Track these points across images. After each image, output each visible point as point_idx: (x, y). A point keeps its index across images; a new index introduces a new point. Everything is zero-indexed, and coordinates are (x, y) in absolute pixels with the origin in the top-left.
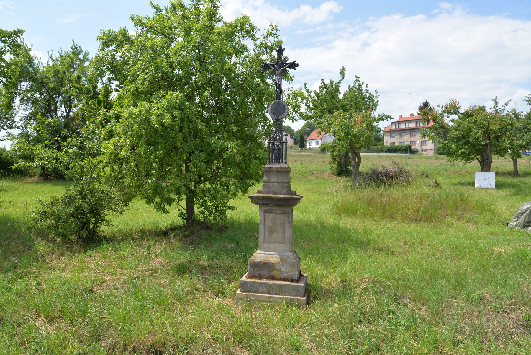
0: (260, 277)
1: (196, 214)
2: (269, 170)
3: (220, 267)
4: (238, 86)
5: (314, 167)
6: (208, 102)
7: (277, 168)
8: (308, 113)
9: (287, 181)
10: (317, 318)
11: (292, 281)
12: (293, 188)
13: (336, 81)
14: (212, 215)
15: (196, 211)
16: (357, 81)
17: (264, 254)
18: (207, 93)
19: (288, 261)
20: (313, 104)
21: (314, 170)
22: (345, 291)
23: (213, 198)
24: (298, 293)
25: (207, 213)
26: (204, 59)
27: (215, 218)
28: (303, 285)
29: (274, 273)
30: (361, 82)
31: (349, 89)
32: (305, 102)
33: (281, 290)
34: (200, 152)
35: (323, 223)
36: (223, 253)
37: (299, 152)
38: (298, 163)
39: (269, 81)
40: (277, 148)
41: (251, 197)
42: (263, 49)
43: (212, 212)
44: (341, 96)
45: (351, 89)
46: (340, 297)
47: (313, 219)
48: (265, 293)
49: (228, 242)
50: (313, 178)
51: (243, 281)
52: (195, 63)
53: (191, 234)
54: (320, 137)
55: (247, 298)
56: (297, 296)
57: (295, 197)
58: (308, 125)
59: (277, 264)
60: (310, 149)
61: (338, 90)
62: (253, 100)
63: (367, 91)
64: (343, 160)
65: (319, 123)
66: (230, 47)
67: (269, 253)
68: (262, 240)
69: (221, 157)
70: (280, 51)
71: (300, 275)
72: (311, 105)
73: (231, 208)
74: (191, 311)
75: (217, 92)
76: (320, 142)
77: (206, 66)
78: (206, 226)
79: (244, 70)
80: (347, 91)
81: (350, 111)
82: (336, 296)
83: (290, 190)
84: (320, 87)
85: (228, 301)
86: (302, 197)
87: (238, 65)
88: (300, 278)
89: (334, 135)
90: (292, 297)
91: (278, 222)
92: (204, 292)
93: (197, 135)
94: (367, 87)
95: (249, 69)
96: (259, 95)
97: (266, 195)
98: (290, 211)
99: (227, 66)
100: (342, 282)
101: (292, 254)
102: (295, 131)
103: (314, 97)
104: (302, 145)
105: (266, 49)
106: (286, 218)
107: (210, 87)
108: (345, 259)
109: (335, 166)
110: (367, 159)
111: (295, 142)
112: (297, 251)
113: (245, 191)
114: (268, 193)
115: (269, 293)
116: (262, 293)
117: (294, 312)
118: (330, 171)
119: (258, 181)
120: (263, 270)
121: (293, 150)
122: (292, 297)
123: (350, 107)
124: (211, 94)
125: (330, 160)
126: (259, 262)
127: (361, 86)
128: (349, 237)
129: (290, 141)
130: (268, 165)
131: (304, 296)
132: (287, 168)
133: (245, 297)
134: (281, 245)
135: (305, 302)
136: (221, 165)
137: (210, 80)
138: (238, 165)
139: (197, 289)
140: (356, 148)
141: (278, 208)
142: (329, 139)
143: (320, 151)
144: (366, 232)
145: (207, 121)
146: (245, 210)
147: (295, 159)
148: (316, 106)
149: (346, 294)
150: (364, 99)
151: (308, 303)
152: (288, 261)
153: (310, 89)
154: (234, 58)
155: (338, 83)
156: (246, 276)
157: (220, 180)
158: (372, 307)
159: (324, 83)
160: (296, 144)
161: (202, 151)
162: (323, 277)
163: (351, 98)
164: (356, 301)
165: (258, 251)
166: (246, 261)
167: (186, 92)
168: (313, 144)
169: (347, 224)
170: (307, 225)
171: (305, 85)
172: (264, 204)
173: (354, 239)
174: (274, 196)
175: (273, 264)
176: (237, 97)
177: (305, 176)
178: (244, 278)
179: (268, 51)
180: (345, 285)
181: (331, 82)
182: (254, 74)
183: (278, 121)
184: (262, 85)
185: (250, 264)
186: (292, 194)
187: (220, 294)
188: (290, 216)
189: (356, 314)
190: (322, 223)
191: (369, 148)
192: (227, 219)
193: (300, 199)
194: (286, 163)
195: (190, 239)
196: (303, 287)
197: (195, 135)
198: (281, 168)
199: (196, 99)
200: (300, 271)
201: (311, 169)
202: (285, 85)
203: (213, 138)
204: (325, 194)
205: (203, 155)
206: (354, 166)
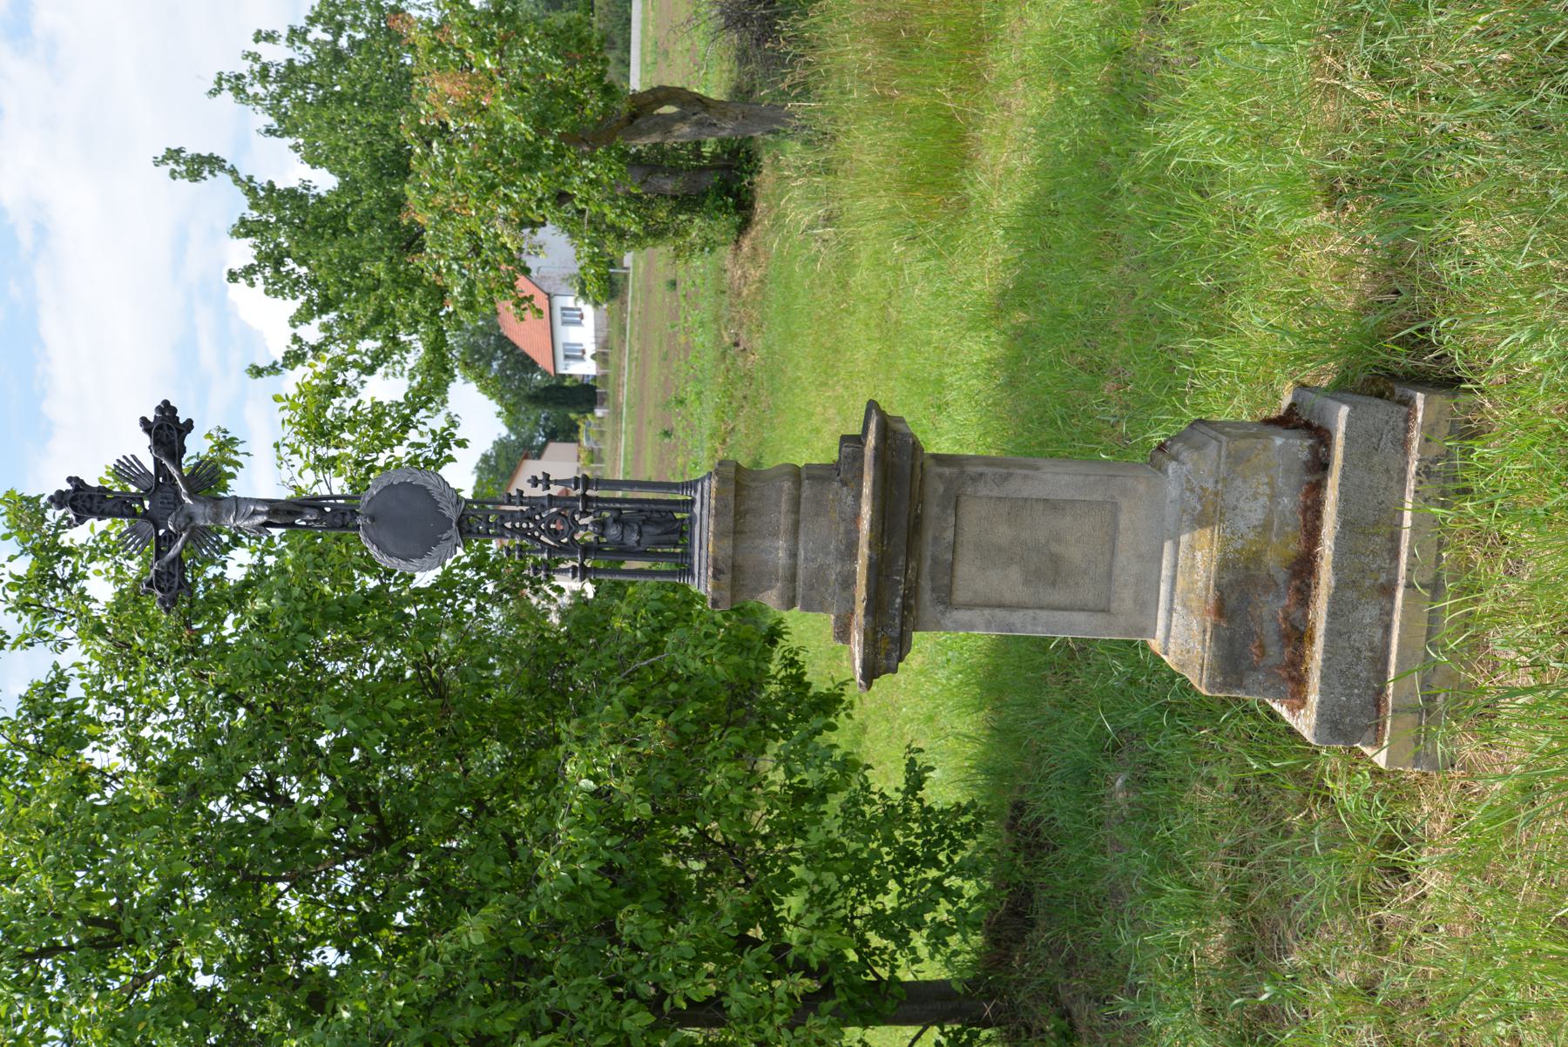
0: (1298, 636)
1: (944, 975)
2: (726, 579)
3: (1242, 851)
4: (261, 734)
5: (701, 339)
6: (342, 900)
7: (719, 535)
8: (412, 360)
9: (787, 485)
10: (1537, 335)
11: (1320, 465)
12: (822, 450)
13: (240, 206)
14: (953, 882)
15: (932, 971)
16: (237, 85)
17: (1170, 611)
18: (292, 905)
19: (1210, 485)
20: (364, 333)
21: (719, 336)
22: (1386, 184)
23: (863, 875)
24: (1387, 438)
25: (943, 912)
26: (97, 922)
27: (970, 869)
28: (1344, 411)
29: (1275, 561)
30: (244, 67)
31: (286, 133)
32: (352, 374)
33: (1371, 528)
34: (616, 941)
35: (1003, 295)
36: (1161, 832)
37: (617, 414)
38: (678, 424)
39: (238, 565)
40: (613, 531)
41: (871, 672)
42: (56, 599)
43: (937, 882)
44: (324, 181)
45: (285, 126)
46: (1423, 208)
47: (979, 348)
48: (1390, 613)
49: (1098, 800)
50: (758, 343)
51: (1319, 726)
52: (115, 974)
53: (1056, 1002)
54: (540, 301)
55: (1416, 711)
56: (1405, 444)
57: (871, 441)
58: (476, 361)
59: (1225, 542)
60: (601, 357)
61: (291, 193)
62: (341, 651)
63: (296, 35)
64: (669, 185)
65: (469, 306)
66: (38, 777)
67: (1164, 588)
68: (1099, 619)
69: (638, 830)
70: (82, 500)
71: (1288, 421)
72: (368, 344)
73: (916, 779)
74: (1501, 1028)
75: (294, 852)
76: (569, 302)
77: (138, 915)
78: (1010, 921)
79: (175, 699)
80: (296, 148)
81: (408, 134)
82: (1414, 233)
83: (835, 468)
84: (274, 291)
85: (1430, 812)
86: (872, 405)
87: (146, 733)
88: (1308, 426)
89: (534, 225)
90: (1413, 468)
91: (1003, 533)
92: (1381, 945)
93: (523, 959)
94: (270, 37)
95: (167, 677)
96: (316, 622)
97: (861, 592)
98: (947, 471)
99: (150, 794)
100: (1333, 197)
101: (1172, 467)
102: (504, 431)
103: (326, 328)
104: (585, 395)
105: (54, 582)
106: (983, 490)
107: (258, 888)
108: (1204, 179)
109: (697, 227)
110: (662, 52)
111: (567, 433)
112: (1157, 437)
113: (829, 704)
114: (848, 582)
115: (1388, 590)
116: (1387, 629)
117: (1503, 459)
118: (726, 252)
119: (773, 635)
120: (1257, 617)
121: (606, 447)
122: (1413, 468)
123: (386, 136)
124: (300, 882)
125: (661, 252)
126: (1216, 637)
127: (265, 69)
128: (1082, 158)
129: (561, 463)
130: (702, 585)
131: (1408, 403)
132: (722, 481)
133: (1411, 718)
134: (1124, 520)
135: (1440, 399)
136: (685, 831)
137: (222, 888)
138: (688, 742)
139: (1369, 989)
140: (606, 111)
141: (929, 535)
142: (555, 252)
143: (616, 304)
144: (1060, 67)
145: (449, 903)
146: (926, 707)
147: (651, 435)
148: (378, 319)
149: (1406, 177)
150: (338, 57)
151: (1450, 383)
152: (1210, 485)
153: (277, 345)
154: (105, 757)
155: (251, 191)
156: (1291, 710)
157: (764, 838)
158: (1489, 35)
159: (249, 271)
160: (575, 428)
161: (609, 930)
162: (1299, 302)
163: (333, 128)
164: (1447, 120)
165: (1156, 644)
166: (1208, 710)
167: (281, 1022)
168: (576, 341)
169: (1010, 172)
170: (1012, 383)
171: (257, 372)
172: (906, 606)
173: (1098, 131)
174: (864, 551)
175: (1224, 565)
176: (321, 742)
177: (747, 386)
178: (1305, 722)
179: (62, 571)
180: (1351, 182)
181: (245, 229)
182: (195, 648)
183: (470, 521)
184: (260, 604)
185: (1224, 686)
186: (858, 457)
187: (1394, 856)
188: (971, 470)
189: (1525, 119)
190: (1004, 302)
191: (607, 41)
192: (973, 804)
193: (883, 416)
194: (691, 485)
195: (1083, 1011)
196: (1354, 407)
197: (527, 966)
198: (718, 514)
199: (325, 968)
200: (1268, 422)
201: (711, 354)
202: (261, 478)
203: (542, 872)
204: (845, 285)
205: (629, 921)
206: (700, 124)
